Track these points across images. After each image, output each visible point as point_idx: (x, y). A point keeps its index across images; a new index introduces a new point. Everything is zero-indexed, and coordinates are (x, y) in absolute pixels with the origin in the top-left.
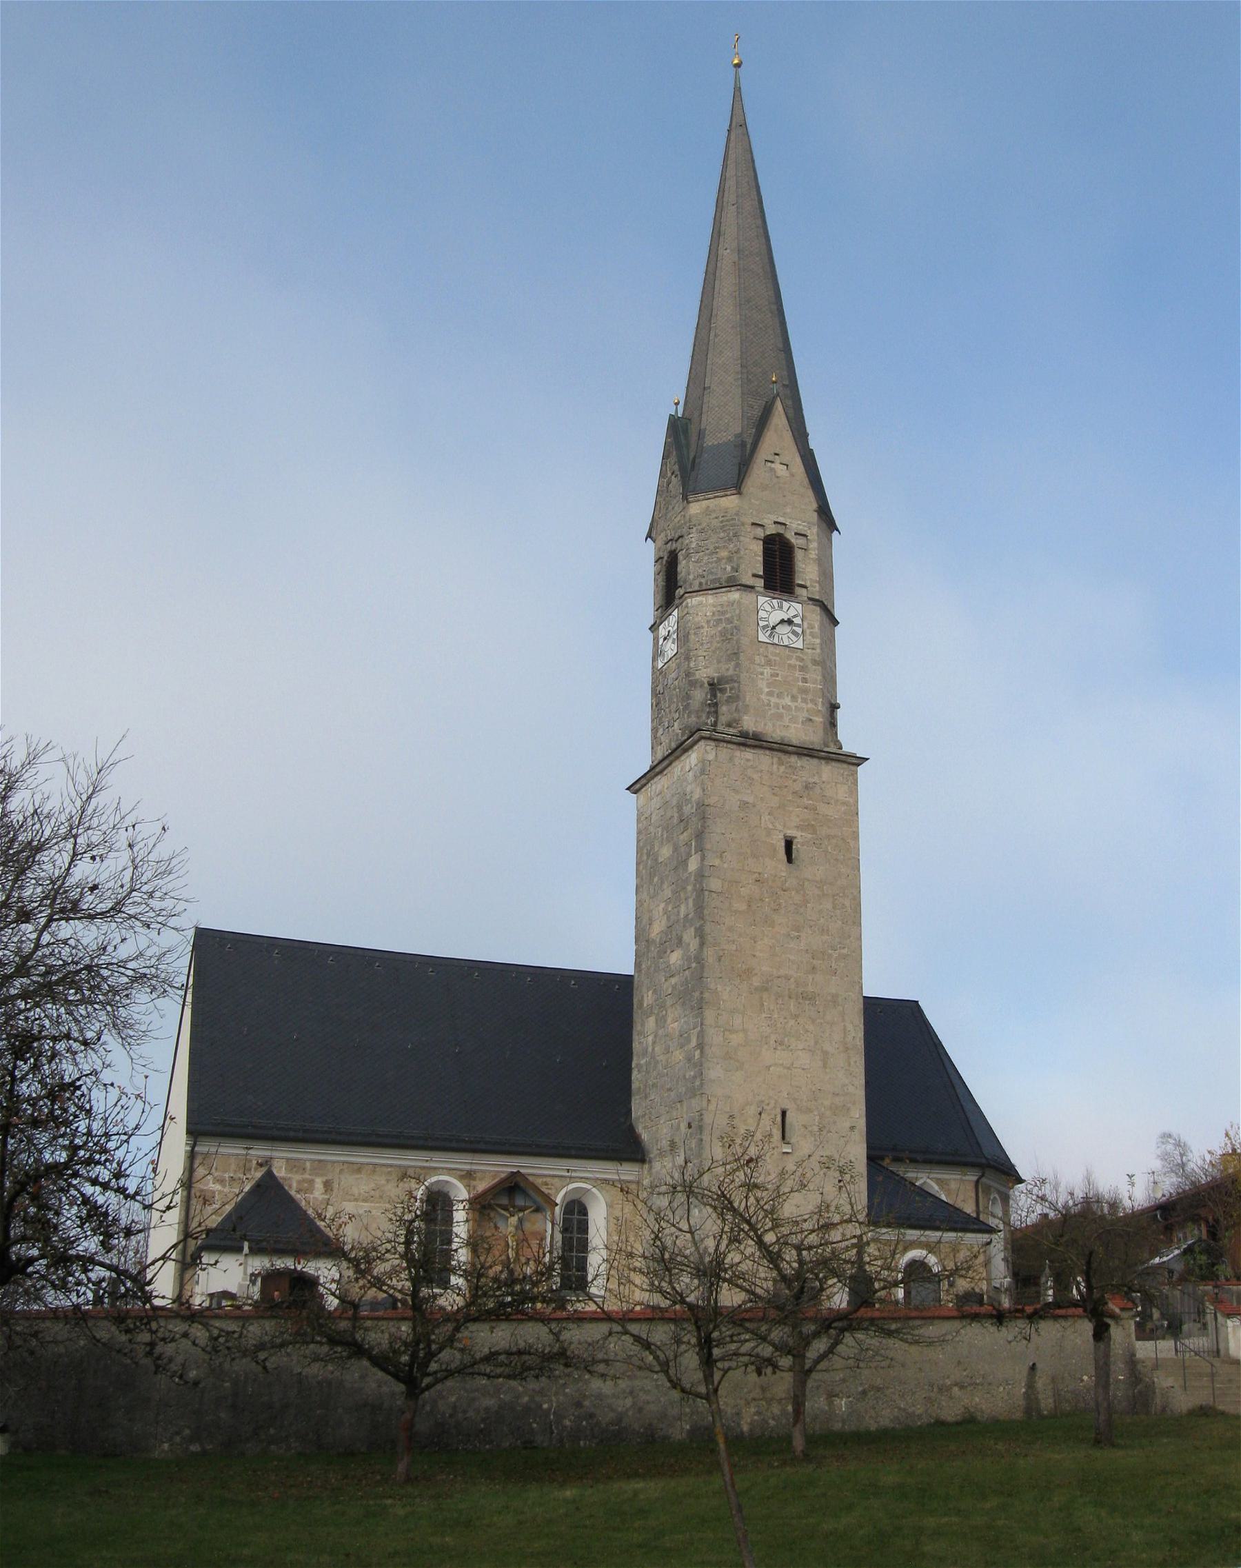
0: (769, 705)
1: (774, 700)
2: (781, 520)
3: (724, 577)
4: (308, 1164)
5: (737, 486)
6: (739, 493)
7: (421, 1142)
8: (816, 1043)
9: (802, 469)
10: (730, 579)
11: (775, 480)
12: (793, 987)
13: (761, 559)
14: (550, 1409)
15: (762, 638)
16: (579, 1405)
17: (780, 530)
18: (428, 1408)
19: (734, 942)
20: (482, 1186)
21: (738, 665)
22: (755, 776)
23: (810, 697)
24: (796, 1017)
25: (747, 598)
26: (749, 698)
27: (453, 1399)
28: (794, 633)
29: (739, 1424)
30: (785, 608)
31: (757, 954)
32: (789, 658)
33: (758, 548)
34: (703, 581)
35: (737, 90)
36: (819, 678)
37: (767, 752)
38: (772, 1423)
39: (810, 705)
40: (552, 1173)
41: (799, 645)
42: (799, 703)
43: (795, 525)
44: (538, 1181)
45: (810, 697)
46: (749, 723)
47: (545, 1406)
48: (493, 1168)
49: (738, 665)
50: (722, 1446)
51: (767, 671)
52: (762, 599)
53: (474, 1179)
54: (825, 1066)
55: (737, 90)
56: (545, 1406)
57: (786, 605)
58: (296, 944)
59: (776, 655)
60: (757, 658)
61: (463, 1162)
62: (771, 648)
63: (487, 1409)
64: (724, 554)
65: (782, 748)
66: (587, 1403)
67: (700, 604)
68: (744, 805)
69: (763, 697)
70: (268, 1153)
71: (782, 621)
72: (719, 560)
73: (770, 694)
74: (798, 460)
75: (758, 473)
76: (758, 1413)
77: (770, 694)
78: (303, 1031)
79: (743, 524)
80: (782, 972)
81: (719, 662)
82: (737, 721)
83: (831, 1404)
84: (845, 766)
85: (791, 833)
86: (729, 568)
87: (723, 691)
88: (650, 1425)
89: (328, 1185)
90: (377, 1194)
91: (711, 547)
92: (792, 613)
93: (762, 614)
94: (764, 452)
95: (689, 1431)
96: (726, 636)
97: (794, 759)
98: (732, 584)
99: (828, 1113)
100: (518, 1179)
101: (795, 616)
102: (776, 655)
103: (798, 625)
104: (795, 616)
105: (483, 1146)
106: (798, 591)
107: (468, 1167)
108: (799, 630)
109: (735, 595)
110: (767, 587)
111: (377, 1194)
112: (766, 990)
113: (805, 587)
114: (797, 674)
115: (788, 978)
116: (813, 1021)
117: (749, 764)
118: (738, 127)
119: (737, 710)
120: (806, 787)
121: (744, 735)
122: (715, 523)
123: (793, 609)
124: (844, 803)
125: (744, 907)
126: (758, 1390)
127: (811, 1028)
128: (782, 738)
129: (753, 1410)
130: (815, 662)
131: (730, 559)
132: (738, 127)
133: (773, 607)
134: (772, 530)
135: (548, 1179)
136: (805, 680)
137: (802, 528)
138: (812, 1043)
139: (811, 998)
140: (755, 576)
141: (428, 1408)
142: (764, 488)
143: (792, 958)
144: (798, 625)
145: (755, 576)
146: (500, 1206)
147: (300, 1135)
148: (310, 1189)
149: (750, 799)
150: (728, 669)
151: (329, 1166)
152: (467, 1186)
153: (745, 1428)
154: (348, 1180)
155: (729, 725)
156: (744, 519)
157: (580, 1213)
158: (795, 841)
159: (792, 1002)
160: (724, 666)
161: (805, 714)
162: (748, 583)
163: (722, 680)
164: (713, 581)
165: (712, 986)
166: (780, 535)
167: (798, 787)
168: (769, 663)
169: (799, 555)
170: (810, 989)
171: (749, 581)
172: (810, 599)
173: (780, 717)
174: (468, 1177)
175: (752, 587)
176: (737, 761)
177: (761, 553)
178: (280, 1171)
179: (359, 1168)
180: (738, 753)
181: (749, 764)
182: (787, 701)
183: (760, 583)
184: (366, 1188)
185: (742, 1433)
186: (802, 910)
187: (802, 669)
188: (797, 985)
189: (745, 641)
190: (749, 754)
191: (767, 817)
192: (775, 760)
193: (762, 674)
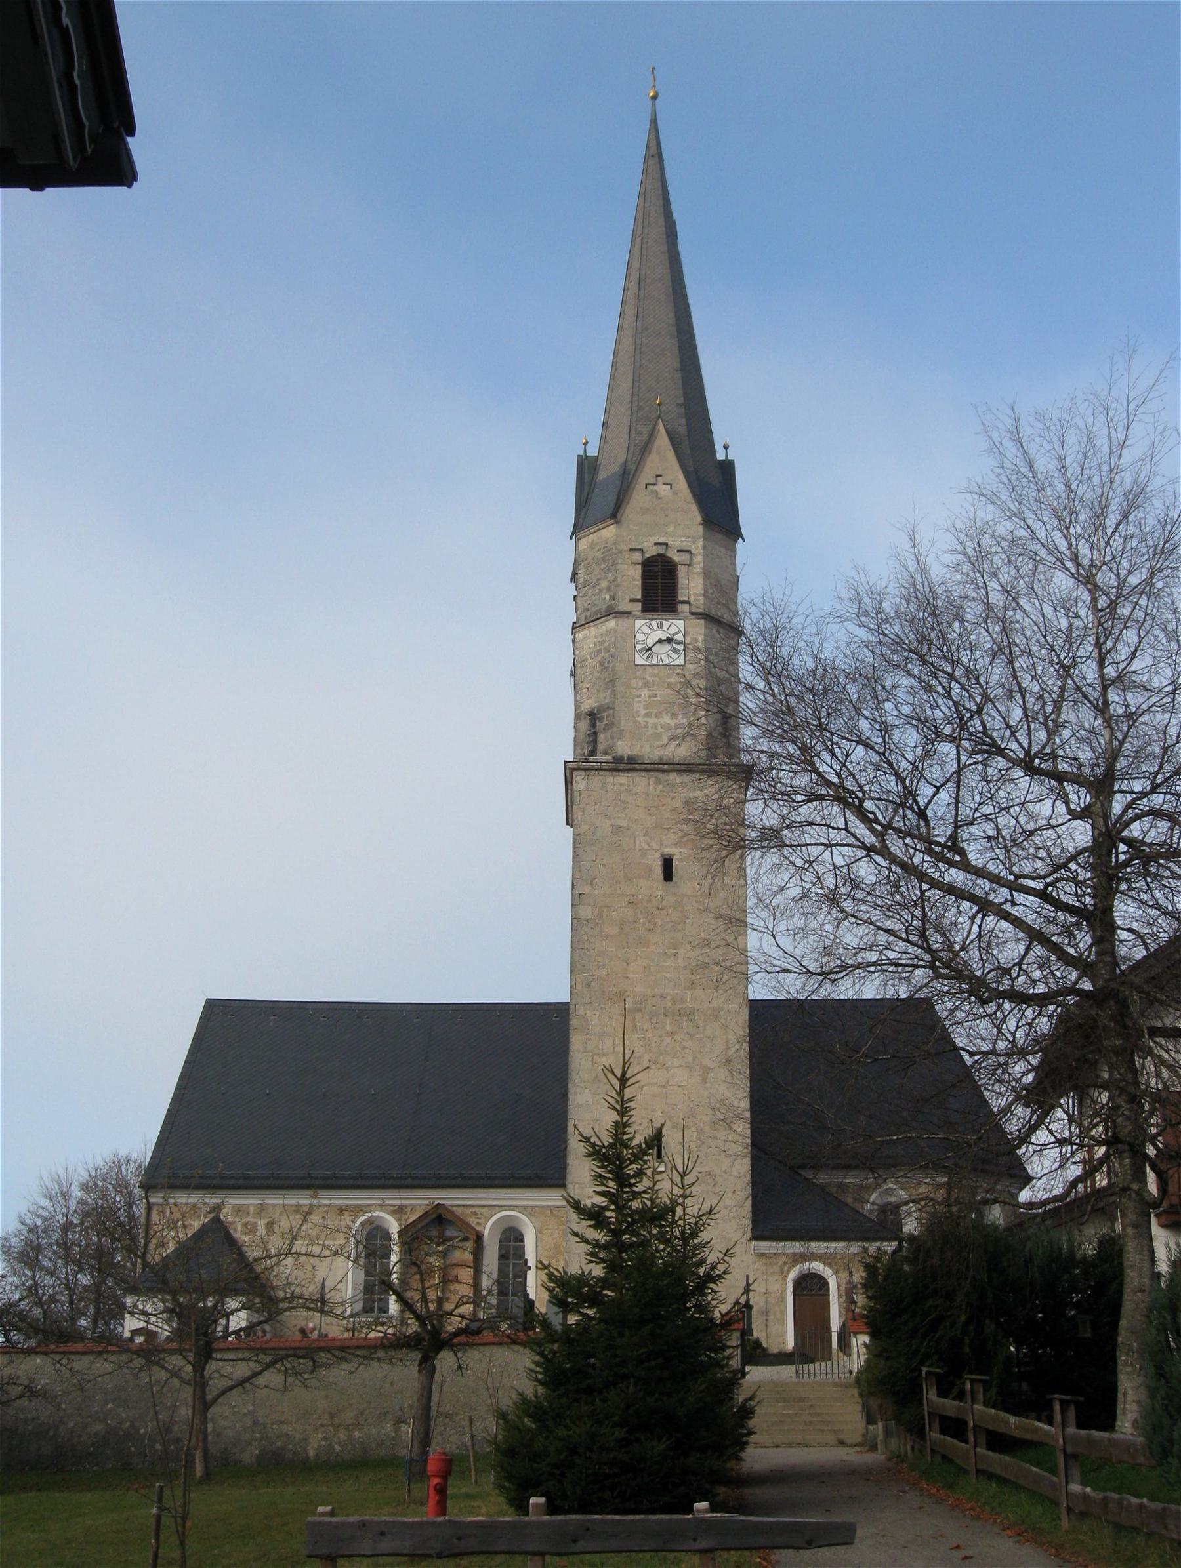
0: (646, 726)
1: (651, 721)
2: (662, 540)
3: (604, 607)
4: (252, 1208)
5: (615, 515)
6: (617, 522)
7: (351, 1182)
8: (695, 1059)
9: (686, 486)
10: (610, 607)
12: (669, 1004)
13: (639, 583)
14: (145, 1433)
15: (639, 660)
17: (661, 550)
18: (51, 1433)
19: (604, 966)
21: (613, 692)
22: (630, 800)
24: (672, 1034)
25: (626, 623)
26: (624, 723)
27: (71, 1424)
28: (675, 651)
29: (305, 1450)
30: (665, 628)
31: (630, 975)
33: (636, 573)
34: (588, 614)
35: (654, 122)
37: (643, 774)
38: (338, 1448)
40: (514, 1203)
43: (676, 543)
44: (458, 1211)
46: (624, 748)
47: (142, 1431)
48: (419, 1201)
49: (613, 692)
51: (645, 693)
53: (406, 1213)
54: (704, 1081)
55: (654, 122)
56: (142, 1431)
57: (666, 624)
58: (486, 1007)
59: (655, 675)
61: (394, 1198)
62: (649, 670)
63: (96, 1434)
64: (604, 584)
66: (176, 1428)
67: (586, 637)
68: (617, 829)
69: (640, 719)
71: (660, 641)
72: (600, 591)
73: (648, 715)
74: (681, 477)
75: (639, 498)
76: (325, 1439)
77: (648, 715)
79: (620, 552)
80: (657, 991)
81: (598, 691)
82: (611, 748)
83: (397, 1430)
85: (667, 851)
86: (608, 597)
87: (601, 719)
88: (226, 1449)
91: (594, 580)
92: (673, 630)
93: (639, 637)
94: (646, 475)
95: (257, 1456)
96: (604, 666)
97: (672, 777)
98: (612, 612)
99: (707, 1128)
100: (440, 1211)
101: (677, 633)
102: (655, 675)
103: (679, 642)
104: (677, 633)
105: (409, 1181)
106: (681, 607)
107: (398, 1202)
109: (611, 623)
112: (639, 1010)
113: (688, 602)
115: (663, 997)
116: (692, 1037)
117: (623, 788)
118: (655, 156)
119: (612, 737)
121: (618, 760)
122: (598, 555)
123: (674, 626)
125: (615, 930)
126: (326, 1416)
127: (688, 1043)
128: (661, 758)
129: (320, 1436)
131: (608, 589)
132: (655, 156)
133: (652, 629)
134: (652, 551)
135: (477, 1210)
138: (690, 1059)
139: (689, 1014)
140: (632, 601)
141: (51, 1433)
142: (644, 511)
143: (668, 975)
144: (679, 642)
145: (632, 601)
146: (429, 1238)
147: (241, 1182)
149: (624, 824)
150: (604, 697)
151: (271, 1208)
152: (399, 1220)
153: (311, 1453)
155: (606, 753)
157: (383, 1238)
158: (674, 858)
159: (668, 1020)
160: (602, 695)
162: (626, 609)
163: (602, 708)
164: (595, 613)
165: (581, 1012)
166: (661, 556)
168: (647, 685)
169: (682, 571)
170: (689, 1004)
171: (624, 606)
172: (692, 614)
174: (399, 1211)
175: (629, 613)
176: (610, 787)
177: (639, 578)
178: (227, 1214)
180: (611, 779)
181: (623, 788)
183: (638, 606)
185: (308, 1457)
186: (679, 927)
188: (674, 1001)
189: (621, 667)
190: (623, 779)
191: (642, 839)
192: (652, 780)
193: (639, 696)
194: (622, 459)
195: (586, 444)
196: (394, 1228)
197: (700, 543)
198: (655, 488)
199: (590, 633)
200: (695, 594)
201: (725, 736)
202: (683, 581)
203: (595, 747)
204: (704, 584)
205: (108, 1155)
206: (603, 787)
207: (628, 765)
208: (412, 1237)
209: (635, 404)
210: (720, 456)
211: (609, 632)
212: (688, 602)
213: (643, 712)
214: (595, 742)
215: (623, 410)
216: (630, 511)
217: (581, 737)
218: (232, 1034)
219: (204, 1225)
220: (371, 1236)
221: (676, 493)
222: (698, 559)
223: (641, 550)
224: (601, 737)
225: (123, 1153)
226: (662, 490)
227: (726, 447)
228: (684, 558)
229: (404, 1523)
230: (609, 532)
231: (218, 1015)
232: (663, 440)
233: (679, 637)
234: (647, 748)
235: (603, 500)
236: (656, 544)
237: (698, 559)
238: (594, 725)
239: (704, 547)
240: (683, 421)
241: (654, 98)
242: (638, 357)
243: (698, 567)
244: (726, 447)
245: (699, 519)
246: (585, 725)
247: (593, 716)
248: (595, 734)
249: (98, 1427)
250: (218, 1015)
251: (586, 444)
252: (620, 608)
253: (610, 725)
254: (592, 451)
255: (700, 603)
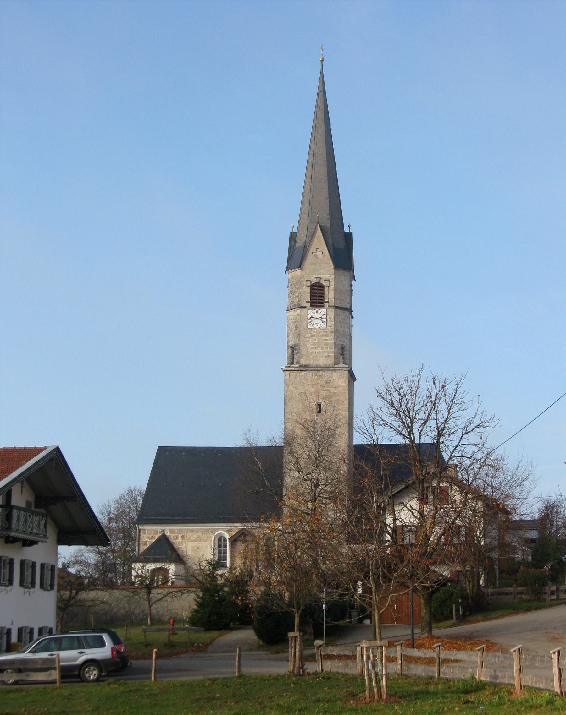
1: (313, 350)
6: (301, 269)
10: (299, 304)
11: (317, 260)
13: (309, 294)
15: (309, 326)
16: (143, 612)
17: (318, 280)
20: (233, 533)
21: (299, 339)
22: (305, 382)
23: (329, 346)
25: (304, 311)
26: (303, 352)
28: (323, 322)
32: (320, 332)
33: (308, 290)
36: (333, 338)
39: (329, 350)
41: (325, 326)
42: (325, 350)
45: (329, 346)
46: (303, 362)
48: (237, 527)
49: (299, 339)
50: (377, 617)
51: (311, 339)
52: (309, 311)
57: (319, 311)
59: (315, 332)
60: (307, 335)
62: (313, 330)
64: (297, 294)
65: (317, 369)
69: (309, 350)
70: (163, 528)
73: (312, 348)
75: (310, 258)
77: (312, 348)
78: (189, 481)
79: (302, 282)
84: (343, 371)
87: (295, 349)
89: (183, 537)
90: (199, 539)
92: (322, 313)
94: (312, 249)
96: (296, 327)
97: (321, 372)
102: (315, 332)
108: (325, 320)
109: (299, 311)
110: (311, 306)
111: (199, 539)
113: (328, 302)
114: (324, 338)
120: (326, 383)
121: (301, 366)
123: (322, 312)
124: (342, 386)
128: (317, 365)
130: (331, 332)
131: (298, 296)
132: (322, 91)
134: (314, 281)
136: (327, 340)
137: (327, 278)
140: (307, 302)
142: (311, 264)
145: (307, 302)
148: (177, 538)
154: (189, 535)
156: (302, 279)
161: (327, 354)
167: (323, 383)
168: (312, 336)
169: (326, 289)
172: (329, 306)
173: (316, 357)
174: (229, 531)
175: (305, 307)
176: (298, 377)
179: (192, 531)
180: (298, 374)
182: (319, 350)
184: (196, 537)
187: (326, 336)
189: (302, 329)
190: (303, 374)
194: (304, 240)
195: (293, 227)
196: (227, 537)
197: (333, 277)
198: (316, 253)
199: (292, 313)
200: (331, 298)
201: (342, 354)
202: (326, 293)
203: (293, 360)
204: (335, 294)
205: (126, 488)
206: (295, 377)
207: (305, 368)
208: (234, 540)
209: (310, 215)
210: (346, 230)
211: (298, 315)
212: (328, 302)
213: (311, 347)
214: (293, 358)
215: (305, 216)
216: (307, 264)
217: (289, 356)
218: (167, 459)
219: (160, 537)
220: (220, 540)
221: (324, 256)
222: (332, 284)
223: (310, 281)
224: (296, 356)
225: (132, 487)
226: (319, 254)
227: (349, 226)
228: (327, 283)
229: (480, 579)
230: (298, 272)
231: (162, 451)
232: (319, 233)
233: (324, 316)
234: (312, 361)
235: (296, 259)
236: (316, 278)
237: (332, 284)
238: (293, 352)
239: (335, 278)
240: (329, 222)
241: (322, 61)
242: (311, 193)
243: (332, 287)
244: (349, 226)
245: (333, 267)
246: (290, 351)
247: (293, 348)
248: (293, 355)
249: (123, 611)
250: (162, 451)
251: (293, 227)
252: (302, 305)
253: (298, 353)
254: (295, 231)
255: (332, 303)
